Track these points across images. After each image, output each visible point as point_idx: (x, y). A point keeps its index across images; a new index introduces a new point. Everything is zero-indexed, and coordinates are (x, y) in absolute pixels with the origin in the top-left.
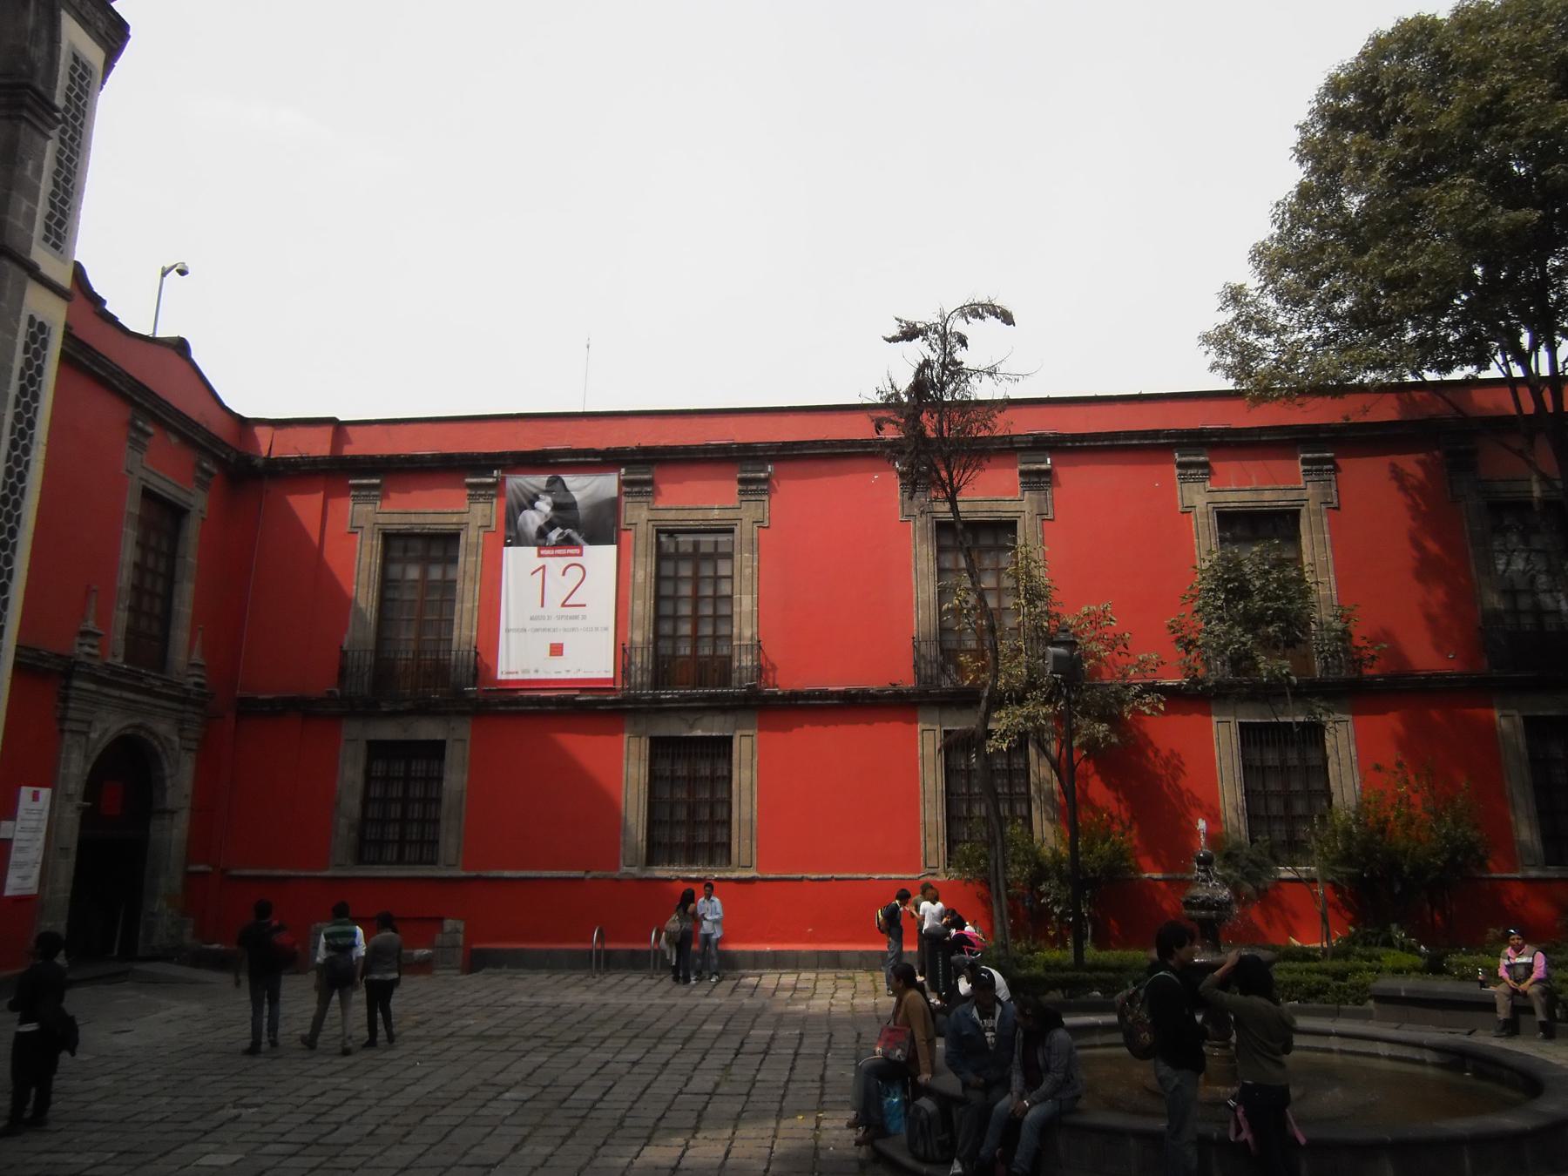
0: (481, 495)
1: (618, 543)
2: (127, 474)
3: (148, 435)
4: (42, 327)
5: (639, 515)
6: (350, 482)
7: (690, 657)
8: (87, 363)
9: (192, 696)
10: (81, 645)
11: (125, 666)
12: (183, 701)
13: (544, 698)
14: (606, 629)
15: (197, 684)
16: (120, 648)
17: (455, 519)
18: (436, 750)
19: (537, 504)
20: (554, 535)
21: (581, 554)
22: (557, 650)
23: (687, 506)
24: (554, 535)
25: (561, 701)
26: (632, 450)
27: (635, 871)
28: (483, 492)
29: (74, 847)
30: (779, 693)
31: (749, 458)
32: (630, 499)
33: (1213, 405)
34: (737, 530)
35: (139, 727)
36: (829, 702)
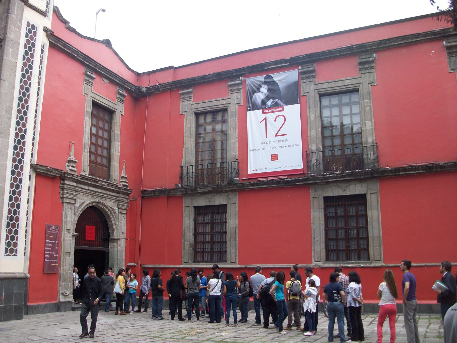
0: (235, 89)
1: (300, 103)
2: (85, 95)
3: (93, 78)
4: (33, 27)
5: (310, 88)
6: (180, 92)
7: (341, 155)
8: (62, 47)
9: (121, 190)
10: (68, 166)
11: (90, 176)
12: (118, 192)
13: (270, 181)
14: (298, 145)
15: (124, 185)
16: (87, 168)
17: (224, 102)
18: (223, 209)
19: (261, 89)
21: (283, 110)
22: (275, 157)
23: (333, 81)
24: (269, 103)
25: (278, 182)
26: (303, 57)
27: (320, 264)
28: (236, 88)
29: (73, 252)
30: (389, 169)
31: (363, 52)
32: (304, 81)
34: (360, 89)
35: (98, 202)
36: (417, 172)
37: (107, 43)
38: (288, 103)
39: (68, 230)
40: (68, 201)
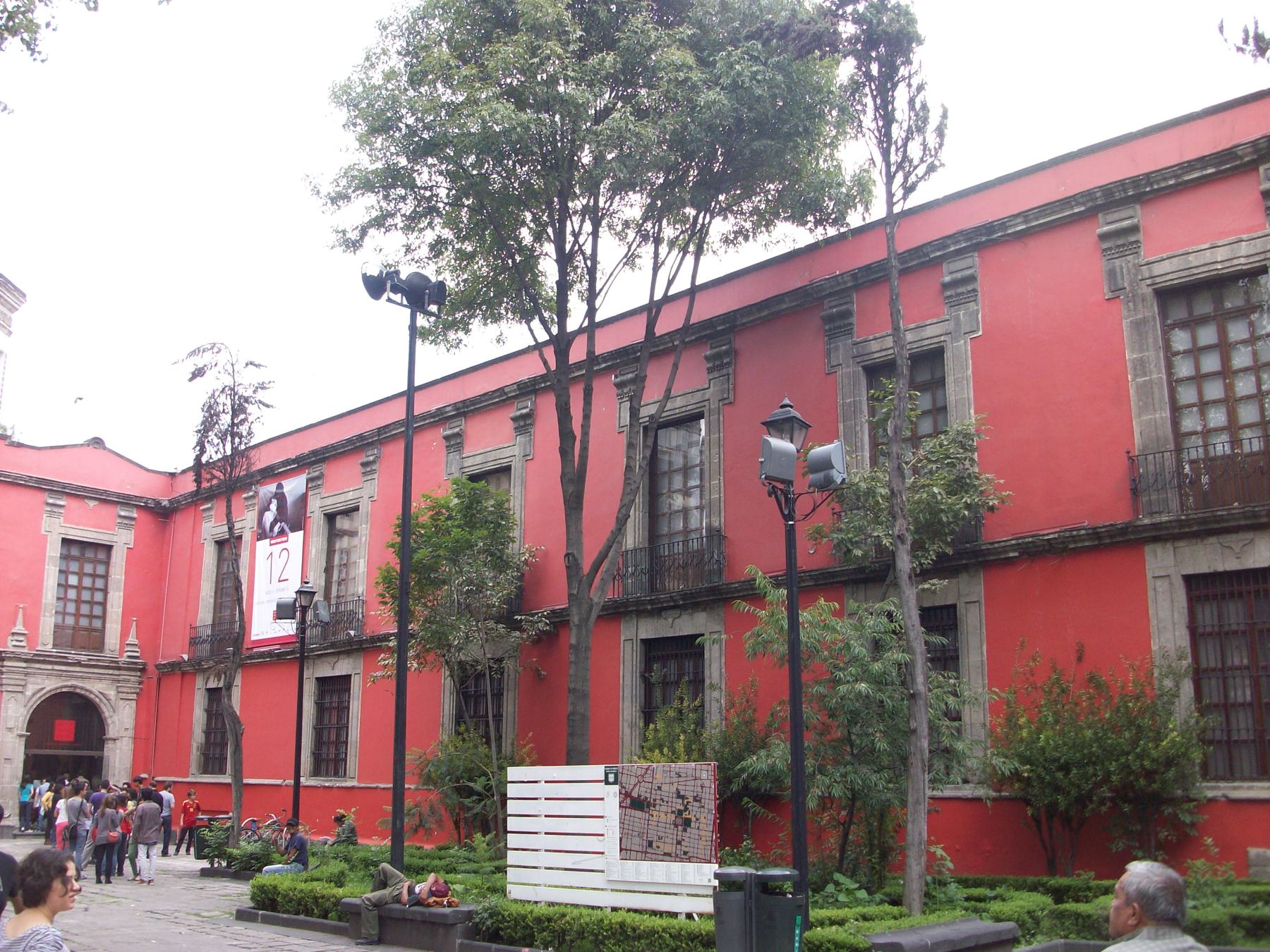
12: (119, 668)
20: (276, 529)
37: (97, 442)
38: (293, 529)
40: (10, 689)
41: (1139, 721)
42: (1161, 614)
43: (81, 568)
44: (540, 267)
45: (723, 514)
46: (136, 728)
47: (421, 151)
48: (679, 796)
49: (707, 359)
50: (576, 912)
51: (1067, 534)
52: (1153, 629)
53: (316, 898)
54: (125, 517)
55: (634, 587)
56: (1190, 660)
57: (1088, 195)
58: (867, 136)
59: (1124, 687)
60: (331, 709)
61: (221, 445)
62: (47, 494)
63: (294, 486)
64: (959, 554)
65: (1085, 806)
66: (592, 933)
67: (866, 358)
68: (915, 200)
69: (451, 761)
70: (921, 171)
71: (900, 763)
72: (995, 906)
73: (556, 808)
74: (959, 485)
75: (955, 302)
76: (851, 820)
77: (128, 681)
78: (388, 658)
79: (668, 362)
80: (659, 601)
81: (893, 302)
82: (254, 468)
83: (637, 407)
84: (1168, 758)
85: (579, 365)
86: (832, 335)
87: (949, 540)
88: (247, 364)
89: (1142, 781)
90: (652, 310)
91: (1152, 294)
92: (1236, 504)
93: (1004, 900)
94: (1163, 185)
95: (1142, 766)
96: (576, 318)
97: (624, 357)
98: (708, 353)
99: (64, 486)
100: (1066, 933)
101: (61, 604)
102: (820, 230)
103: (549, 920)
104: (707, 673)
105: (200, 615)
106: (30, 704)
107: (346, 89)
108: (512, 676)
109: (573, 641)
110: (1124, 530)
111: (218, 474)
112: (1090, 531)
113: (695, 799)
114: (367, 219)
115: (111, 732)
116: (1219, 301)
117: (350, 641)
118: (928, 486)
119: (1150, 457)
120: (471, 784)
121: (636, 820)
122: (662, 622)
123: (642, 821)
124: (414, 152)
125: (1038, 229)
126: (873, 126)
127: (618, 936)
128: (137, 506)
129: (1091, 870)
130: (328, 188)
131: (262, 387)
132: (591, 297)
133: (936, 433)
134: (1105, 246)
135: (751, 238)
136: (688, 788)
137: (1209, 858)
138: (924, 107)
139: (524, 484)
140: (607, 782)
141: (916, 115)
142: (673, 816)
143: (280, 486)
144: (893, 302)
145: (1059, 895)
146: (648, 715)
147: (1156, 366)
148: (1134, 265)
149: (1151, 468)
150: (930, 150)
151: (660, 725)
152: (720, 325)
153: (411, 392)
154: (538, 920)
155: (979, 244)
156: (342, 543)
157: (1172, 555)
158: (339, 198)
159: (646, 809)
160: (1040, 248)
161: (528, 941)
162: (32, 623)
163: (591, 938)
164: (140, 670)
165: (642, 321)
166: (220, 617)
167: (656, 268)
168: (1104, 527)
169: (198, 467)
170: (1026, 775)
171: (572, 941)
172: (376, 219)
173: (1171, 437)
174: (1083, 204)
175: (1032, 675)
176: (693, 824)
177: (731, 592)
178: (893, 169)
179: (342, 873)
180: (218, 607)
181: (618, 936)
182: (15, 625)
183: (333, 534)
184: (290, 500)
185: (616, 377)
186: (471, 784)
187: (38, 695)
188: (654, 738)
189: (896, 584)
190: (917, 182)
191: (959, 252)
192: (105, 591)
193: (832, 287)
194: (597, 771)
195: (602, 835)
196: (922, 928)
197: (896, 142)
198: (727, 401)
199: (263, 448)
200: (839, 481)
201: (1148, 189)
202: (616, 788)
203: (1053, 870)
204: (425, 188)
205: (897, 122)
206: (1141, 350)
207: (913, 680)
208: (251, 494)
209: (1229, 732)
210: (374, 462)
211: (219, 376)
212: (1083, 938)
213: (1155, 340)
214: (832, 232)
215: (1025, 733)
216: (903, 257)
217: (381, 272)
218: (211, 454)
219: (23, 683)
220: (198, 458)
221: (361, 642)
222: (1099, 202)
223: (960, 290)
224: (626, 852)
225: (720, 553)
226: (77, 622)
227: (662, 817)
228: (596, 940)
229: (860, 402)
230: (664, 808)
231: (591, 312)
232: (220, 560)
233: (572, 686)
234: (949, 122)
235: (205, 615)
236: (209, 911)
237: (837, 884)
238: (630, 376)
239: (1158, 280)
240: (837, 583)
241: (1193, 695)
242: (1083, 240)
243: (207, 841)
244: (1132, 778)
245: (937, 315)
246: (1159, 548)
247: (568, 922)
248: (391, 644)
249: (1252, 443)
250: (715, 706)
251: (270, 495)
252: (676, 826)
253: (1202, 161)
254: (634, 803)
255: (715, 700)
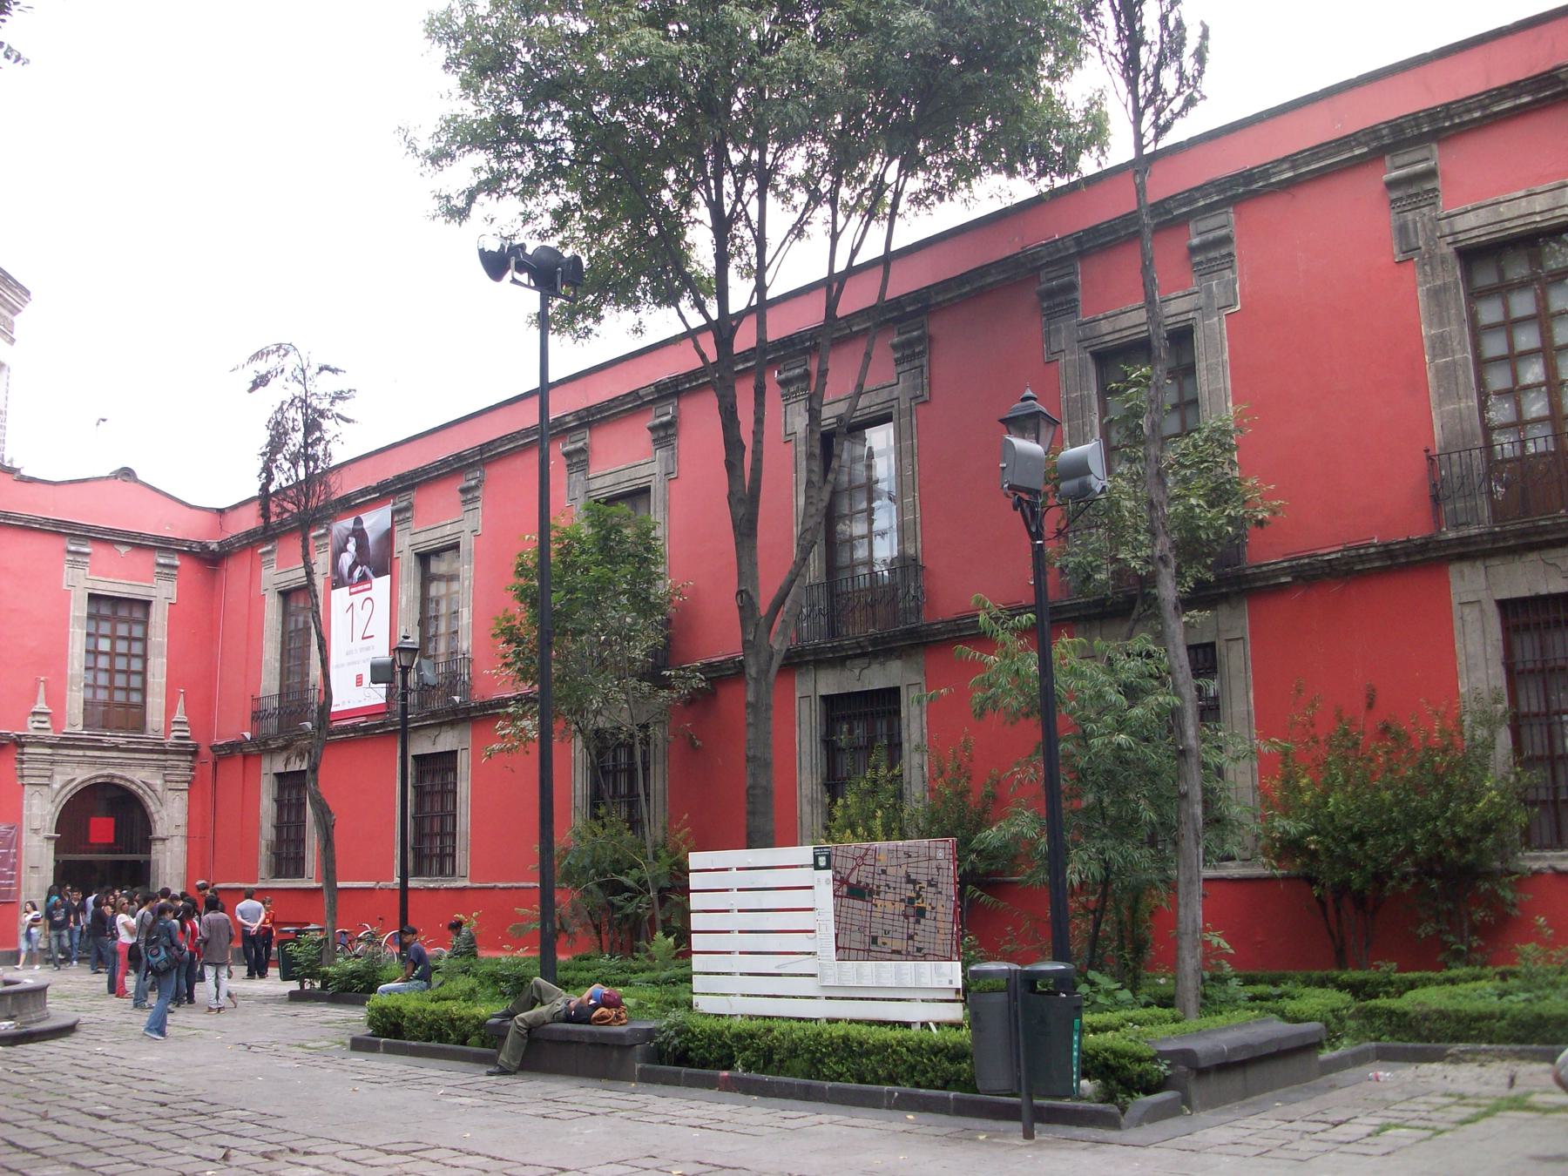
12: (165, 752)
18: (889, 698)
20: (357, 574)
33: (1476, 56)
37: (127, 474)
38: (377, 574)
39: (36, 831)
40: (33, 781)
41: (1448, 779)
42: (1470, 648)
43: (114, 629)
44: (688, 239)
45: (919, 539)
46: (189, 824)
47: (539, 91)
48: (909, 880)
49: (895, 347)
50: (785, 1025)
51: (1353, 553)
52: (1461, 667)
53: (452, 1021)
54: (164, 566)
55: (812, 634)
56: (1506, 704)
57: (1372, 132)
58: (1109, 63)
59: (1428, 737)
60: (432, 793)
61: (293, 471)
62: (67, 539)
63: (376, 520)
64: (1221, 580)
65: (1383, 884)
66: (807, 1050)
67: (1095, 341)
68: (1168, 140)
69: (594, 849)
70: (1177, 105)
71: (1162, 836)
72: (1290, 1006)
73: (752, 900)
74: (1219, 495)
75: (1207, 270)
76: (1103, 908)
77: (177, 767)
78: (508, 726)
79: (860, 347)
80: (842, 648)
81: (1146, 269)
82: (334, 497)
83: (817, 407)
84: (1485, 823)
85: (745, 356)
86: (1052, 314)
87: (1209, 562)
88: (321, 369)
89: (1453, 852)
90: (833, 284)
91: (1454, 255)
92: (1562, 511)
93: (1293, 998)
94: (1466, 118)
95: (1454, 834)
96: (740, 294)
97: (798, 347)
98: (896, 340)
99: (88, 529)
100: (1377, 1034)
101: (91, 674)
102: (1045, 180)
103: (752, 1036)
104: (904, 735)
105: (264, 684)
106: (58, 800)
107: (446, 20)
108: (660, 746)
109: (750, 697)
110: (1424, 546)
111: (290, 506)
112: (1381, 549)
113: (930, 884)
114: (474, 183)
115: (159, 830)
116: (1536, 260)
117: (455, 709)
118: (1185, 496)
119: (1455, 456)
120: (623, 878)
121: (855, 911)
122: (847, 673)
123: (863, 913)
124: (533, 95)
125: (1308, 177)
126: (1117, 50)
127: (841, 1053)
128: (178, 551)
129: (1391, 961)
130: (426, 145)
131: (339, 396)
132: (760, 271)
133: (1185, 432)
134: (1394, 195)
135: (946, 197)
136: (920, 870)
137: (1541, 942)
138: (1180, 25)
139: (667, 508)
140: (817, 867)
141: (1170, 35)
142: (903, 904)
143: (358, 521)
144: (1146, 269)
145: (1358, 990)
146: (833, 785)
147: (1459, 343)
148: (1431, 219)
149: (1456, 469)
150: (1188, 79)
151: (851, 799)
152: (910, 305)
153: (544, 390)
154: (738, 1037)
155: (1234, 197)
156: (436, 589)
157: (1483, 576)
158: (438, 158)
159: (867, 898)
160: (1312, 200)
161: (725, 1063)
162: (56, 699)
163: (806, 1056)
164: (192, 753)
165: (820, 298)
166: (288, 686)
167: (835, 237)
168: (1397, 543)
169: (265, 497)
170: (1313, 847)
171: (781, 1061)
172: (487, 182)
173: (1479, 431)
174: (1366, 144)
175: (1313, 726)
176: (928, 915)
177: (935, 635)
178: (1142, 103)
179: (473, 990)
180: (285, 673)
181: (841, 1053)
182: (35, 702)
183: (426, 579)
184: (372, 538)
185: (779, 373)
186: (623, 878)
187: (69, 788)
188: (844, 814)
189: (1158, 616)
190: (1173, 119)
191: (1210, 208)
192: (144, 657)
193: (1050, 254)
194: (804, 853)
195: (812, 931)
196: (1211, 1031)
197: (1145, 69)
198: (921, 400)
199: (344, 471)
200: (1098, 489)
201: (1447, 124)
202: (829, 873)
203: (1342, 966)
204: (546, 142)
205: (1146, 43)
206: (1441, 324)
207: (1182, 734)
208: (322, 531)
209: (1556, 789)
210: (476, 487)
211: (287, 385)
212: (1399, 1040)
213: (1459, 314)
214: (1060, 182)
215: (1307, 797)
216: (1159, 207)
217: (502, 246)
218: (280, 480)
219: (49, 774)
220: (264, 488)
221: (468, 710)
222: (1386, 141)
223: (1212, 255)
224: (844, 951)
225: (916, 588)
226: (111, 696)
227: (889, 906)
228: (813, 1057)
229: (1089, 396)
230: (890, 896)
231: (761, 288)
232: (286, 614)
233: (751, 753)
234: (1211, 44)
235: (269, 683)
236: (314, 1041)
237: (1092, 984)
238: (797, 371)
239: (1461, 237)
240: (1065, 619)
241: (1511, 747)
242: (1368, 186)
243: (295, 958)
244: (1441, 848)
245: (1183, 287)
246: (1466, 567)
247: (776, 1038)
248: (511, 710)
249: (1539, 443)
250: (916, 774)
251: (347, 533)
252: (906, 917)
253: (1515, 88)
254: (851, 891)
255: (915, 765)
